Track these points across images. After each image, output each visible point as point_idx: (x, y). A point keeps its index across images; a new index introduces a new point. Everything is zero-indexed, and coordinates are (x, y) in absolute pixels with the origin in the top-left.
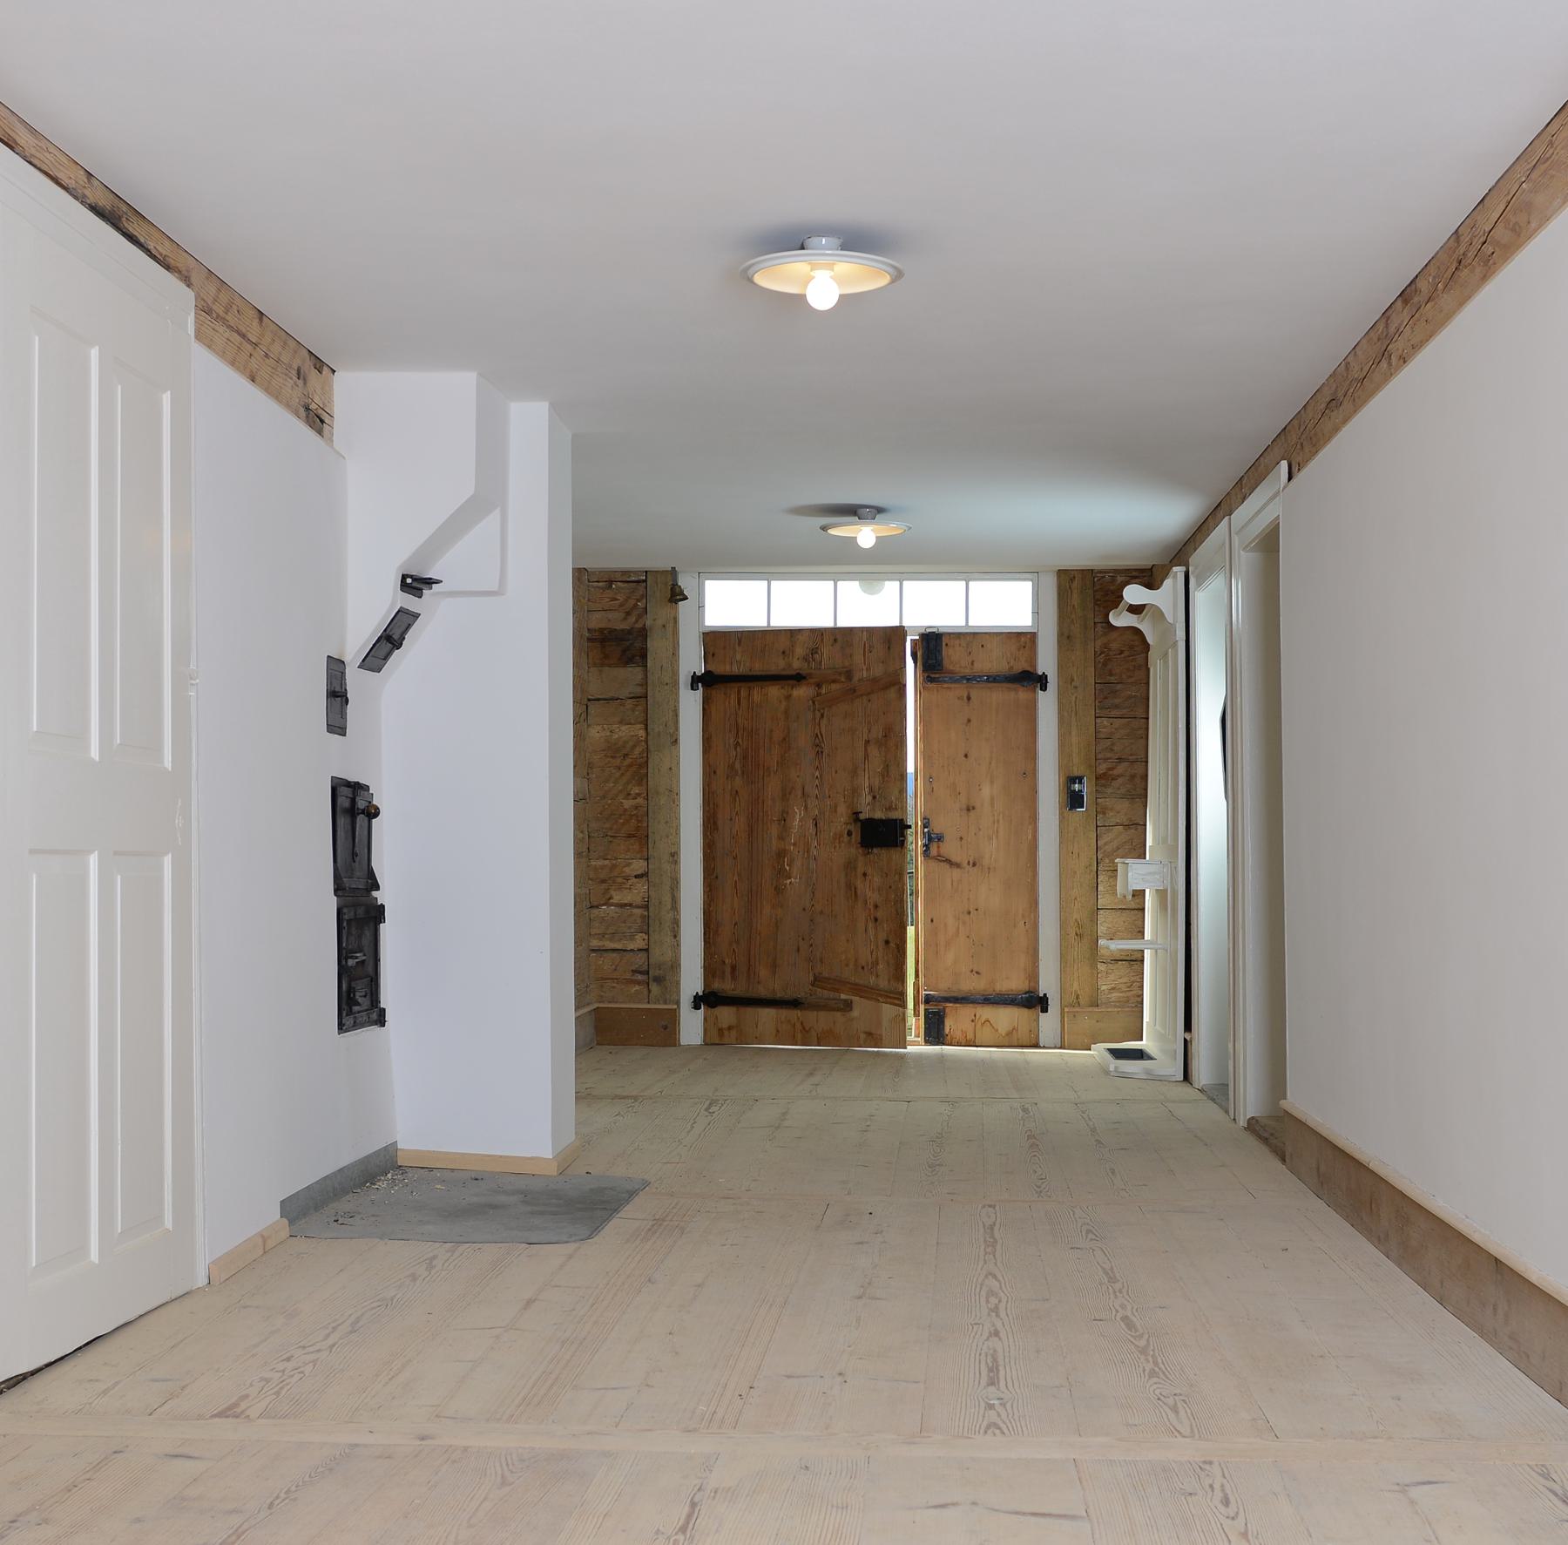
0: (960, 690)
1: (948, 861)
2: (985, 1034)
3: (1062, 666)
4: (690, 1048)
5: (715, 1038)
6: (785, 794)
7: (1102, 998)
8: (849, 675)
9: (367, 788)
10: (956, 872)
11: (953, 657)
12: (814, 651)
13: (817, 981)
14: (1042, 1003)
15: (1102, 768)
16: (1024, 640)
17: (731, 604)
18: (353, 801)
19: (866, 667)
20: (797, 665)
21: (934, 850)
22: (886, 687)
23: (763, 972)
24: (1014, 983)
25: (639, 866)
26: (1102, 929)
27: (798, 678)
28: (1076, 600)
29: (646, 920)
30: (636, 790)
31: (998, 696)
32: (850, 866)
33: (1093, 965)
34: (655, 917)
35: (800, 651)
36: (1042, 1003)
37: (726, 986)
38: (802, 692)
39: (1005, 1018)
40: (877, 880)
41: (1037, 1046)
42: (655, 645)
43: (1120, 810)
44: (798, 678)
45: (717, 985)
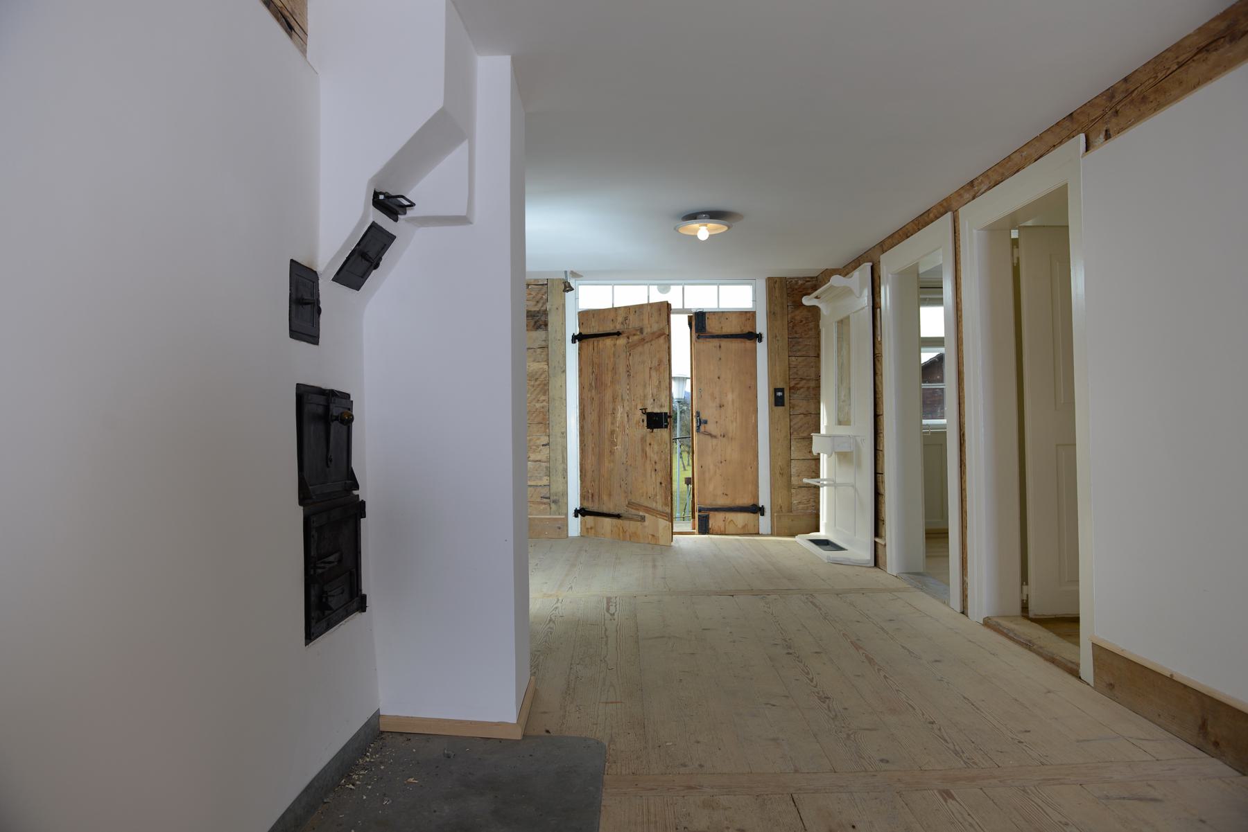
0: (716, 342)
1: (710, 435)
2: (731, 528)
3: (769, 329)
4: (573, 538)
5: (586, 531)
6: (614, 399)
7: (794, 508)
8: (641, 330)
9: (347, 396)
10: (715, 441)
11: (712, 326)
12: (626, 319)
13: (630, 504)
14: (761, 511)
15: (792, 384)
16: (749, 316)
17: (592, 297)
18: (327, 408)
19: (651, 326)
20: (619, 327)
21: (702, 428)
22: (659, 336)
23: (605, 498)
24: (746, 501)
25: (544, 440)
26: (793, 471)
27: (618, 334)
28: (777, 293)
29: (548, 469)
30: (543, 398)
31: (735, 345)
32: (643, 439)
33: (789, 491)
34: (556, 468)
35: (620, 319)
36: (761, 511)
37: (590, 506)
38: (621, 341)
39: (741, 519)
40: (656, 447)
41: (758, 534)
42: (552, 319)
43: (802, 406)
44: (618, 334)
45: (586, 505)
